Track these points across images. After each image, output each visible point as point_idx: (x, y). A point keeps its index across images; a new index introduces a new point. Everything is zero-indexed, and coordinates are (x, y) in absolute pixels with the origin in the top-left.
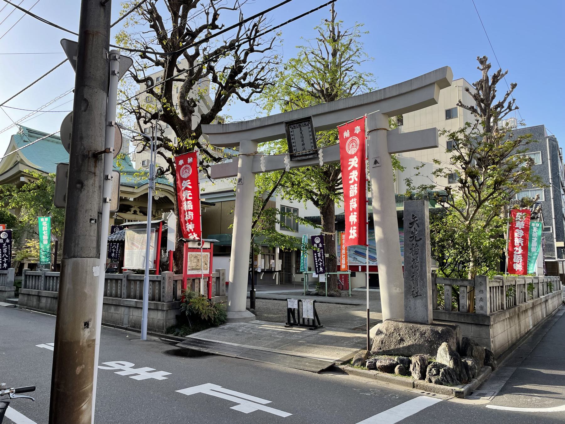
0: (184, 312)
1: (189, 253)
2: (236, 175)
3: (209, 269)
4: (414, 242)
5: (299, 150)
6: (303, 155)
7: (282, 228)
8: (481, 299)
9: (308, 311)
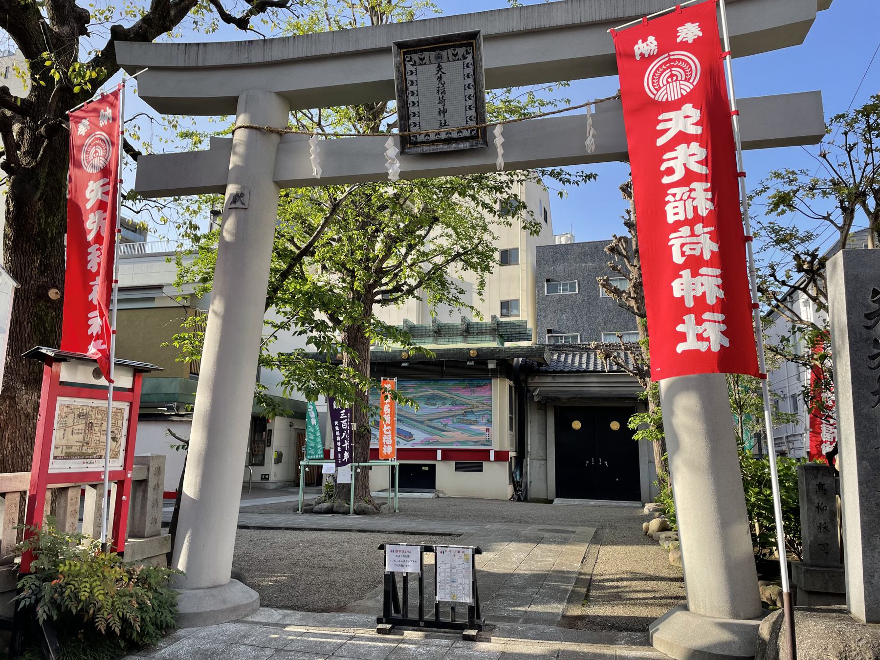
0: (31, 610)
1: (60, 400)
2: (222, 190)
3: (122, 455)
5: (427, 123)
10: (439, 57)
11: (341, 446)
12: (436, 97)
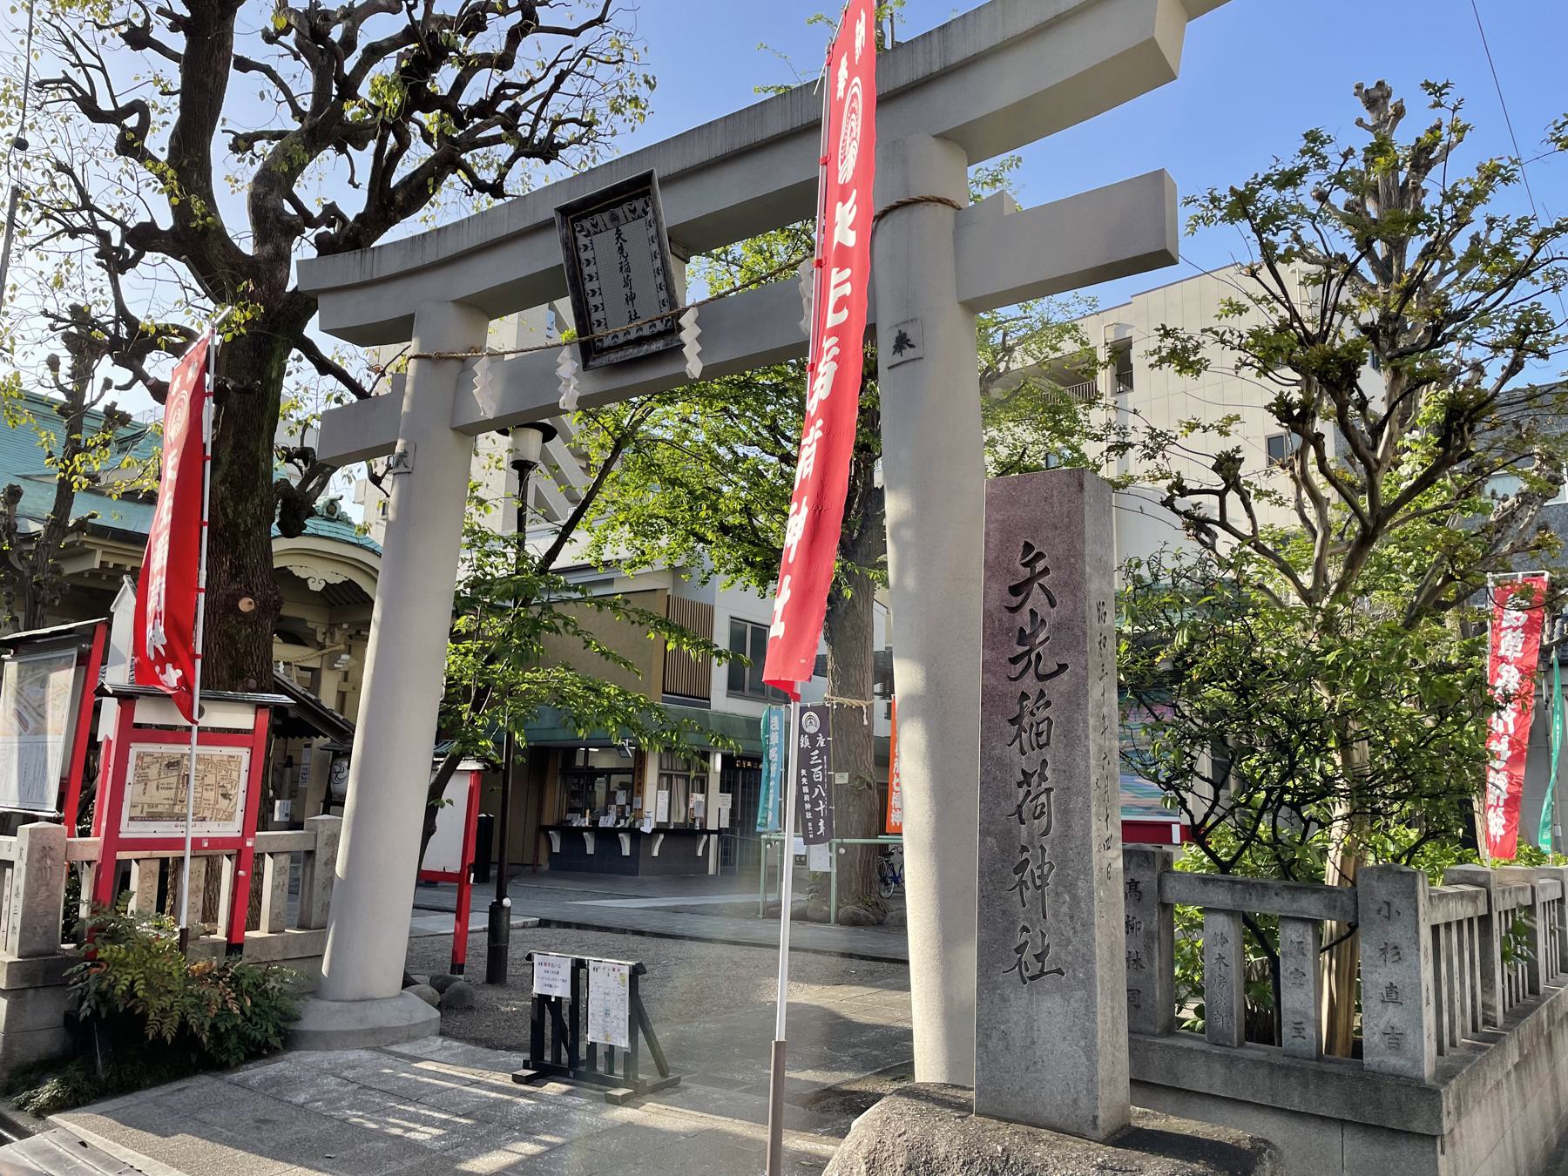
4: (1029, 683)
5: (614, 324)
6: (629, 343)
7: (735, 686)
8: (1392, 994)
9: (607, 1013)
10: (614, 218)
11: (811, 810)
12: (621, 277)
